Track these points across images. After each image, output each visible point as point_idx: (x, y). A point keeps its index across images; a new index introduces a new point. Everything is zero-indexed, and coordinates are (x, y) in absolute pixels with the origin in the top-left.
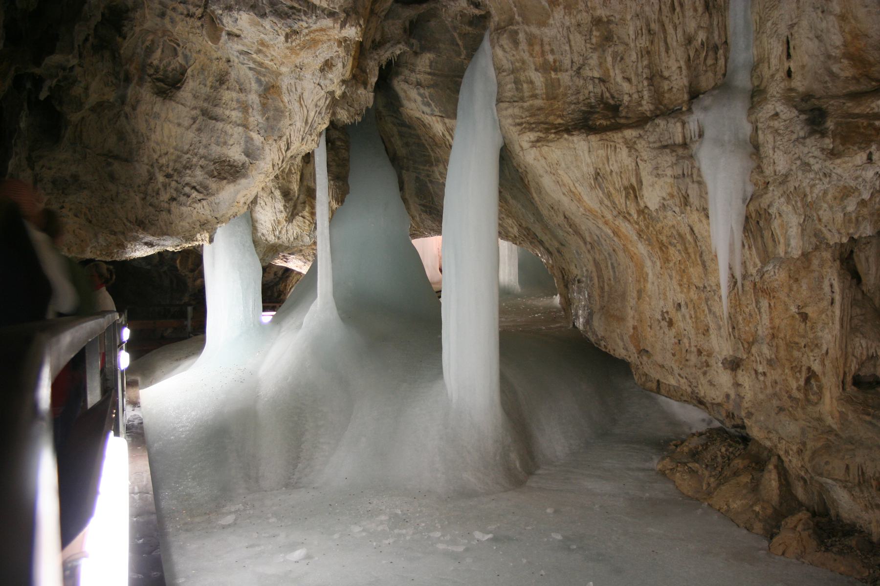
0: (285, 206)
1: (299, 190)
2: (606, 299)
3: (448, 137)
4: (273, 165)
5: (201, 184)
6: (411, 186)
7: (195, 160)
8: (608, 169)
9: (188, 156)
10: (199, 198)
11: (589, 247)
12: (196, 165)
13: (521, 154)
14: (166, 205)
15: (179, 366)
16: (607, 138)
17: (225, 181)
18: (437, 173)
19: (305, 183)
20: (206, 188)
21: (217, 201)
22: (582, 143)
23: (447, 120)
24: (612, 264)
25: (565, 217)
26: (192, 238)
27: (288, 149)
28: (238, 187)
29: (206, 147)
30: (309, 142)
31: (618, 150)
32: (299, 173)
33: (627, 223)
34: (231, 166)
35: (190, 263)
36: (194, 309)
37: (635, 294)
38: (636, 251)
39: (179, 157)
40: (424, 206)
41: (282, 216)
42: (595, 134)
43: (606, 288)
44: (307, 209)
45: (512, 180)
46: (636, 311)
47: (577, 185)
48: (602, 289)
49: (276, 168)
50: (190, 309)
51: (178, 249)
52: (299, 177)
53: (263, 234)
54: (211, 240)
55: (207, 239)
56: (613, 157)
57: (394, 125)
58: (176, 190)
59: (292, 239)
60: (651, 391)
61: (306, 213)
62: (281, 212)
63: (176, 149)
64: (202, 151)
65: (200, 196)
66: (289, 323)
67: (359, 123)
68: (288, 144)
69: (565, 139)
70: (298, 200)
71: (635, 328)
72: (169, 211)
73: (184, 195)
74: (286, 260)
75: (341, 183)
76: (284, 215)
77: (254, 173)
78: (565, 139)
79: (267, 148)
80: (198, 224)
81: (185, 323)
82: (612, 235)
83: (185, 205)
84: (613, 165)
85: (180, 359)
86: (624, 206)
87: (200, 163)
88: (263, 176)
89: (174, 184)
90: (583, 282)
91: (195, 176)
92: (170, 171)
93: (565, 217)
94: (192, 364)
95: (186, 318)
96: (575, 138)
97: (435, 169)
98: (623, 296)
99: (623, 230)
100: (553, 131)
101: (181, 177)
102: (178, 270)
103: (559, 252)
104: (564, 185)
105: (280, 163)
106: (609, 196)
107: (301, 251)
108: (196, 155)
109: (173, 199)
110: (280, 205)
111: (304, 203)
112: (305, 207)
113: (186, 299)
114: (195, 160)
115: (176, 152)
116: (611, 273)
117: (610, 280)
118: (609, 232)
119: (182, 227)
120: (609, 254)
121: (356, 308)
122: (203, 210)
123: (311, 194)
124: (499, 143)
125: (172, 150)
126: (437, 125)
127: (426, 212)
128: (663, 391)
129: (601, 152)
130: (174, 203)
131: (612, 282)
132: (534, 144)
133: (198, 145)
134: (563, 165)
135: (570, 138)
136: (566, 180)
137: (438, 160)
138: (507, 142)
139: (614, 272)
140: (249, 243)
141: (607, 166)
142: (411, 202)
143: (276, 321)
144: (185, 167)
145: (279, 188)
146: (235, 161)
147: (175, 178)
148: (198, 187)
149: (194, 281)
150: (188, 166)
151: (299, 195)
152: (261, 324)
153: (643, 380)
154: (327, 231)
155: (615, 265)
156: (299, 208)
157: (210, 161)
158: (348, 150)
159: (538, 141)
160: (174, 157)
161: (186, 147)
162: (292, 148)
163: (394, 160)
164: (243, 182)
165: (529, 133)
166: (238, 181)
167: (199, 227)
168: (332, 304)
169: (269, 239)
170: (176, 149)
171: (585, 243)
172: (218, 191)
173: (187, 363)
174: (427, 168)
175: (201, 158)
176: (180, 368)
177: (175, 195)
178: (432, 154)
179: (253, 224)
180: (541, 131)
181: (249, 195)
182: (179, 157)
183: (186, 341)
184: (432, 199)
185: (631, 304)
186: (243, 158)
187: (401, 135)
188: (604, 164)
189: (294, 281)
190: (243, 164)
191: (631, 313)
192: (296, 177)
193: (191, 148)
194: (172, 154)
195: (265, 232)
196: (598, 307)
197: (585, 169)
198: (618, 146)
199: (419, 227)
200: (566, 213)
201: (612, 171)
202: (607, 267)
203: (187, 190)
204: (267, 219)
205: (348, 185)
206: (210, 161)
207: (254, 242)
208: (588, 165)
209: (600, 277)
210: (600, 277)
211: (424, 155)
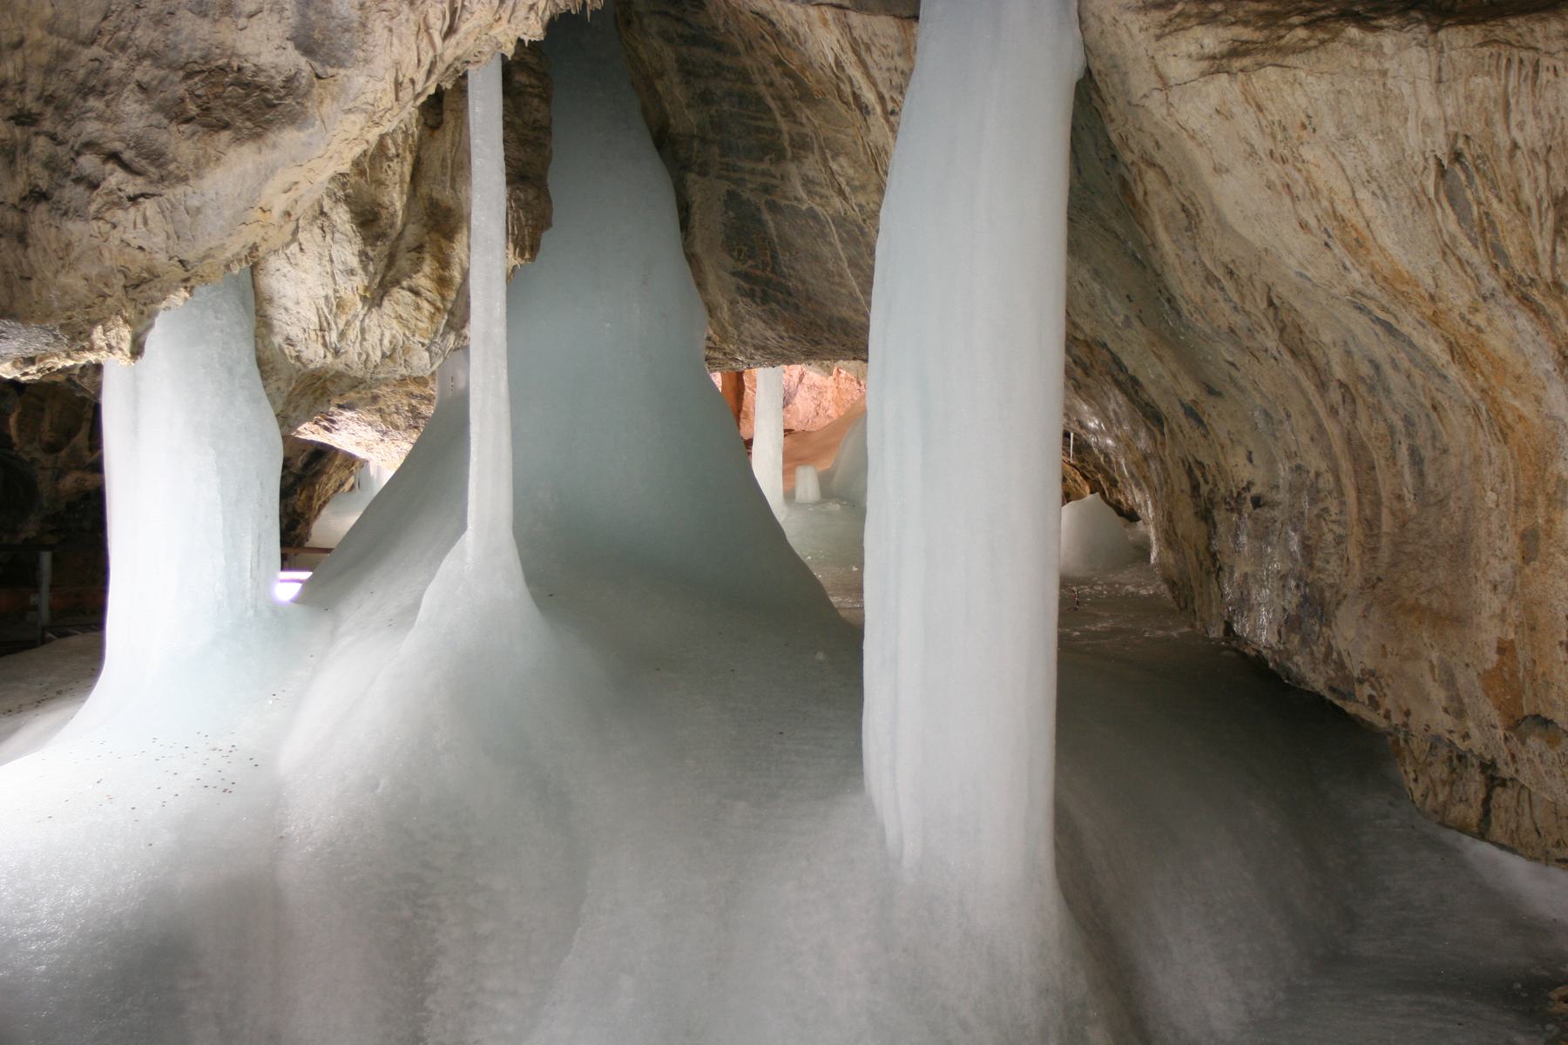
0: (363, 255)
1: (407, 208)
2: (1385, 556)
3: (856, 73)
4: (398, 85)
5: (138, 145)
6: (711, 220)
7: (118, 65)
8: (1503, 140)
9: (96, 51)
10: (131, 190)
11: (1335, 395)
12: (122, 83)
13: (1155, 104)
14: (12, 218)
15: (15, 730)
16: (1511, 36)
17: (225, 136)
18: (797, 182)
19: (424, 190)
20: (157, 157)
21: (194, 202)
22: (1415, 53)
23: (855, 18)
24: (1413, 452)
25: (1271, 303)
26: (78, 336)
27: (451, 31)
28: (269, 156)
29: (158, 21)
30: (522, 12)
31: (1545, 76)
32: (409, 159)
33: (1524, 321)
34: (246, 85)
35: (46, 426)
36: (55, 559)
37: (1510, 545)
38: (1528, 410)
39: (63, 56)
40: (746, 276)
41: (353, 287)
42: (1463, 23)
43: (1387, 523)
44: (427, 269)
45: (1109, 187)
46: (1512, 595)
47: (1363, 194)
48: (1371, 525)
49: (406, 94)
50: (46, 558)
51: (33, 373)
52: (408, 169)
53: (288, 340)
54: (137, 351)
55: (126, 346)
56: (1525, 102)
57: (669, 40)
58: (51, 165)
59: (376, 356)
60: (1463, 829)
61: (423, 281)
62: (352, 272)
63: (51, 28)
64: (144, 36)
65: (133, 186)
66: (366, 607)
67: (595, 13)
68: (453, 12)
69: (1351, 43)
70: (404, 231)
71: (1504, 649)
72: (22, 238)
73: (78, 180)
74: (331, 425)
75: (531, 194)
76: (360, 280)
77: (328, 108)
78: (1351, 43)
79: (378, 25)
80: (119, 281)
81: (33, 599)
82: (1446, 357)
83: (79, 214)
84: (1521, 126)
85: (20, 709)
86: (1545, 260)
87: (137, 75)
88: (359, 119)
89: (41, 145)
90: (1273, 505)
91: (117, 120)
92: (30, 102)
93: (1271, 303)
94: (65, 722)
95: (36, 587)
96: (1388, 41)
97: (792, 168)
98: (1460, 550)
99: (1496, 343)
100: (1295, 20)
101: (69, 123)
102: (11, 446)
103: (1192, 413)
104: (1315, 194)
105: (420, 76)
106: (1484, 230)
107: (375, 398)
108: (123, 47)
109: (38, 196)
110: (347, 251)
111: (419, 248)
112: (420, 261)
113: (30, 529)
114: (118, 65)
115: (54, 40)
116: (1408, 477)
117: (1400, 498)
118: (1438, 352)
119: (65, 291)
120: (1407, 420)
121: (569, 565)
122: (140, 232)
123: (442, 222)
124: (1074, 71)
125: (37, 34)
126: (820, 32)
127: (751, 295)
128: (1496, 831)
129: (1481, 83)
130: (43, 207)
131: (1410, 505)
132: (1217, 64)
133: (129, 15)
134: (1329, 127)
135: (1370, 39)
136: (1327, 175)
137: (802, 145)
138: (1097, 66)
139: (1421, 475)
140: (248, 366)
141: (1499, 128)
142: (708, 265)
143: (308, 596)
144: (85, 90)
145: (347, 199)
146: (259, 70)
147: (47, 125)
148: (128, 155)
149: (60, 474)
150: (97, 86)
151: (405, 225)
152: (276, 609)
153: (1441, 798)
154: (500, 331)
155: (1427, 453)
156: (403, 262)
157: (173, 67)
158: (546, 100)
159: (1234, 53)
160: (43, 57)
161: (88, 24)
162: (464, 28)
163: (663, 140)
164: (289, 137)
165: (1199, 31)
166: (271, 137)
167: (119, 293)
168: (509, 556)
169: (307, 354)
170: (51, 28)
171: (1322, 386)
172: (199, 167)
173: (40, 723)
174: (764, 166)
175: (141, 58)
176: (19, 740)
177: (43, 184)
178: (784, 125)
179: (259, 310)
180: (1246, 24)
181: (304, 187)
182: (63, 56)
183: (33, 653)
184: (774, 257)
185: (1495, 576)
186: (292, 59)
187: (688, 71)
188: (1489, 123)
189: (332, 484)
190: (289, 80)
191: (1491, 603)
192: (398, 172)
193: (108, 26)
194: (39, 46)
195: (295, 332)
196: (1356, 579)
197: (1413, 139)
198: (1545, 62)
199: (725, 337)
200: (1281, 289)
201: (1515, 146)
202: (1393, 458)
203: (89, 163)
204: (303, 295)
205: (549, 201)
206: (173, 67)
207: (260, 363)
208: (1426, 127)
209: (1367, 489)
210: (1367, 489)
211: (758, 130)
